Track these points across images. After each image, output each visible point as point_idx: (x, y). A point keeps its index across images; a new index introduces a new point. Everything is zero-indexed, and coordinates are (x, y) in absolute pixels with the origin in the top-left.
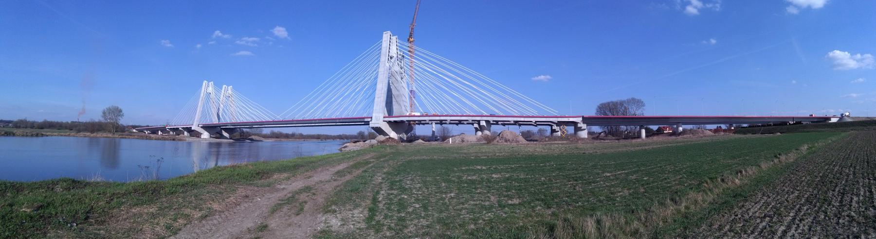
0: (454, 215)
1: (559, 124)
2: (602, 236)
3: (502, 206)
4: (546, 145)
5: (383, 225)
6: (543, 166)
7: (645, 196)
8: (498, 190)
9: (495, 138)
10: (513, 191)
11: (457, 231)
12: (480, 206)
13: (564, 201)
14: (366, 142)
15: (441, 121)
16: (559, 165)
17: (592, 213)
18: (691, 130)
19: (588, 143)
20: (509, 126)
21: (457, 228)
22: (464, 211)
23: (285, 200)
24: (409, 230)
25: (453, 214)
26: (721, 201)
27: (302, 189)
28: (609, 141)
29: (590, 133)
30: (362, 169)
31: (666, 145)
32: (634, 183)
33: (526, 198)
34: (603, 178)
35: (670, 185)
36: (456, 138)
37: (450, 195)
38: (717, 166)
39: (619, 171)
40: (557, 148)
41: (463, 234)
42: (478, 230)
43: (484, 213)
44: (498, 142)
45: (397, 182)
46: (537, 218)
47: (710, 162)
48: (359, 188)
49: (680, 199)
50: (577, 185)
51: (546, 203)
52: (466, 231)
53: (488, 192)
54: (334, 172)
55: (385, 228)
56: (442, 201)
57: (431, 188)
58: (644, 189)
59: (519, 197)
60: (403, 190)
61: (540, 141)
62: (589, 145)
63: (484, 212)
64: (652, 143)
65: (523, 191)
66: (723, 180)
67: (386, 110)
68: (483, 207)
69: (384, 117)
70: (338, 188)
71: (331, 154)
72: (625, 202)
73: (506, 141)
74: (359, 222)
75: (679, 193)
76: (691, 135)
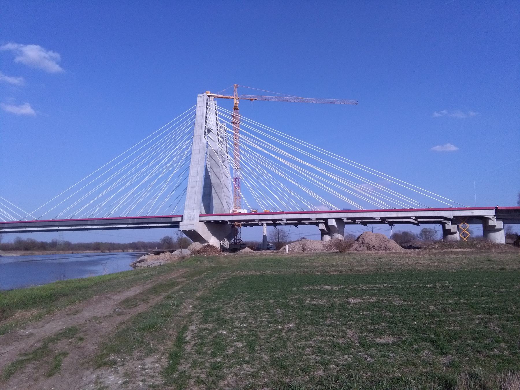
0: (293, 354)
1: (456, 220)
3: (365, 346)
4: (435, 254)
5: (189, 377)
6: (431, 287)
8: (358, 322)
9: (350, 245)
10: (383, 324)
13: (468, 345)
14: (174, 253)
15: (274, 220)
19: (508, 253)
20: (374, 225)
21: (298, 374)
22: (307, 350)
23: (29, 354)
24: (226, 382)
27: (60, 334)
29: (508, 236)
30: (164, 294)
33: (404, 336)
37: (288, 326)
40: (456, 259)
41: (307, 382)
43: (337, 355)
44: (356, 250)
45: (213, 310)
48: (156, 324)
50: (490, 320)
51: (439, 346)
52: (312, 379)
53: (343, 325)
54: (119, 301)
55: (192, 382)
56: (277, 335)
57: (261, 318)
59: (393, 334)
60: (221, 322)
61: (426, 249)
62: (509, 256)
63: (338, 353)
65: (399, 325)
67: (202, 205)
69: (201, 216)
70: (124, 326)
71: (117, 274)
73: (369, 248)
74: (153, 377)
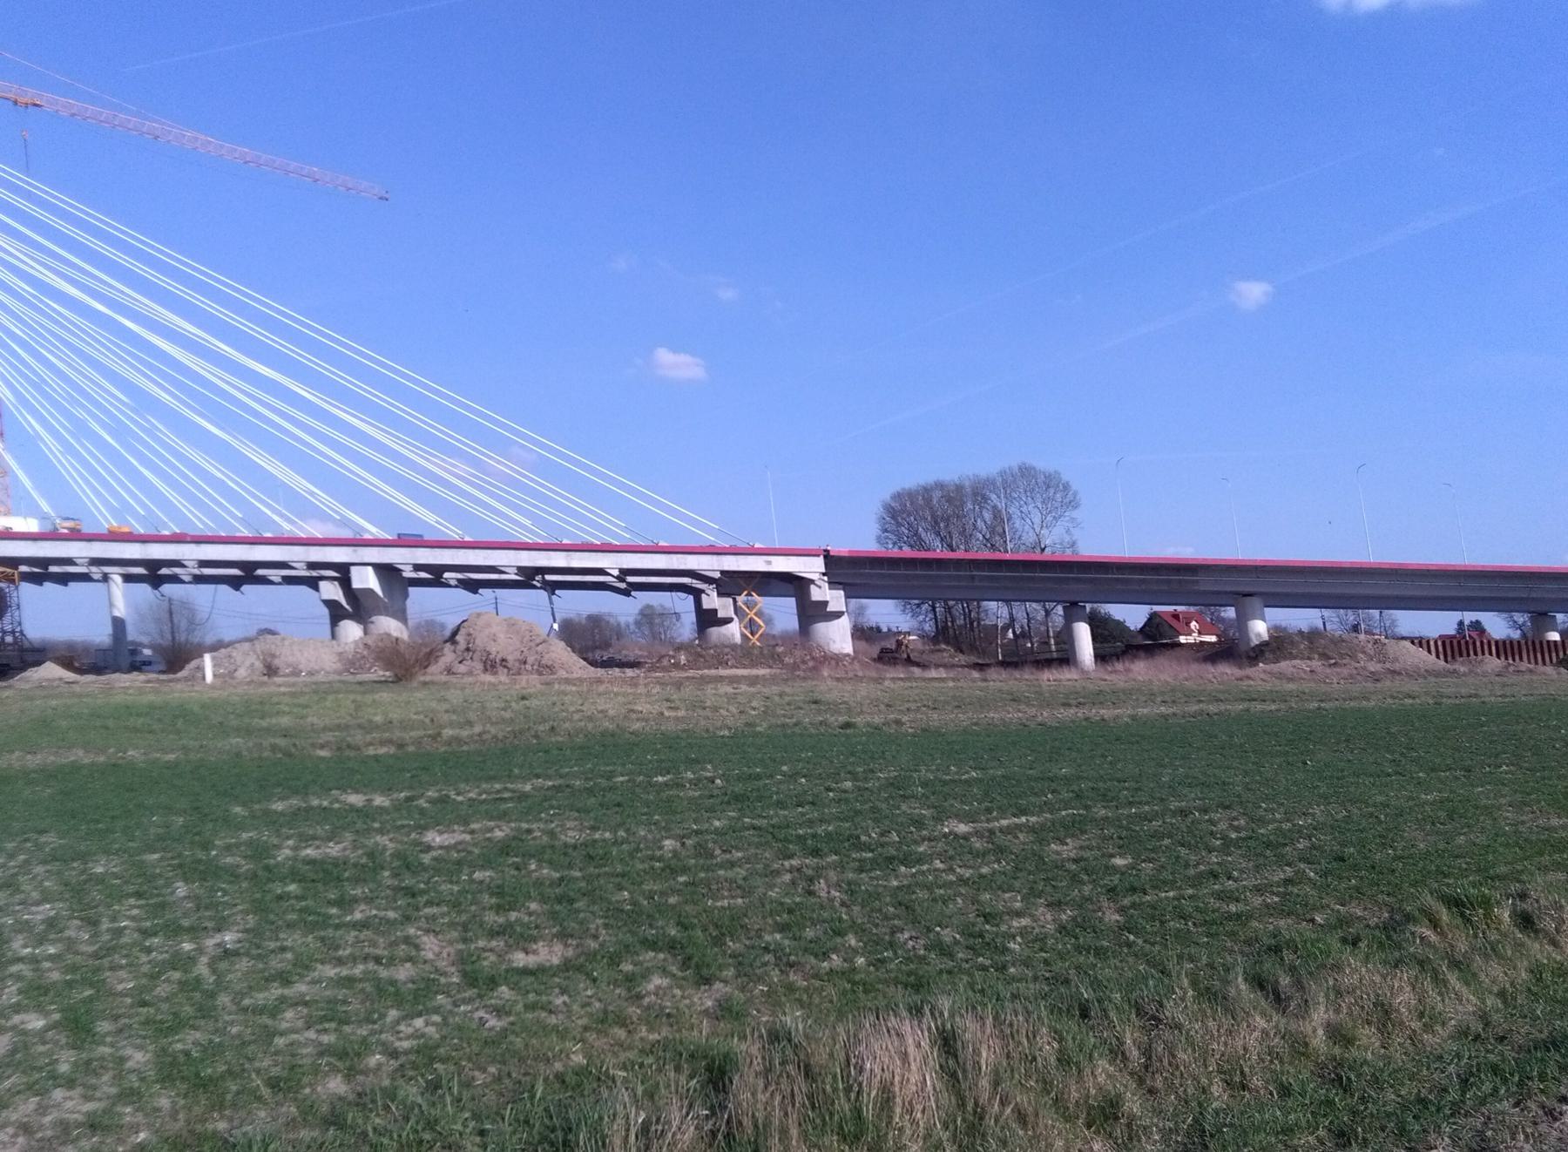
0: (239, 1035)
1: (730, 583)
2: (970, 1108)
3: (478, 981)
6: (666, 784)
7: (1129, 945)
9: (431, 656)
10: (533, 906)
11: (262, 1114)
12: (368, 987)
13: (766, 949)
15: (153, 565)
16: (739, 778)
17: (917, 998)
18: (1312, 636)
19: (861, 679)
20: (500, 592)
21: (259, 1099)
22: (289, 1014)
25: (234, 1030)
26: (1523, 1031)
28: (942, 673)
29: (862, 633)
31: (1195, 708)
32: (1075, 879)
33: (595, 937)
34: (940, 846)
35: (1241, 907)
36: (237, 653)
37: (217, 939)
38: (1482, 839)
39: (1003, 814)
40: (731, 698)
41: (292, 1124)
42: (367, 1099)
43: (388, 1020)
44: (449, 671)
46: (651, 1030)
47: (1442, 814)
49: (1299, 985)
50: (819, 872)
56: (177, 975)
58: (1122, 910)
59: (563, 936)
61: (653, 669)
63: (393, 1014)
64: (1128, 693)
65: (580, 905)
66: (1526, 921)
68: (385, 992)
72: (1046, 962)
73: (490, 665)
75: (1288, 956)
76: (1316, 664)
